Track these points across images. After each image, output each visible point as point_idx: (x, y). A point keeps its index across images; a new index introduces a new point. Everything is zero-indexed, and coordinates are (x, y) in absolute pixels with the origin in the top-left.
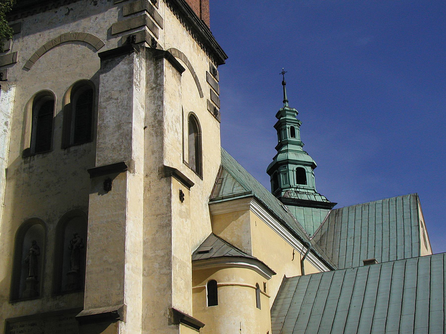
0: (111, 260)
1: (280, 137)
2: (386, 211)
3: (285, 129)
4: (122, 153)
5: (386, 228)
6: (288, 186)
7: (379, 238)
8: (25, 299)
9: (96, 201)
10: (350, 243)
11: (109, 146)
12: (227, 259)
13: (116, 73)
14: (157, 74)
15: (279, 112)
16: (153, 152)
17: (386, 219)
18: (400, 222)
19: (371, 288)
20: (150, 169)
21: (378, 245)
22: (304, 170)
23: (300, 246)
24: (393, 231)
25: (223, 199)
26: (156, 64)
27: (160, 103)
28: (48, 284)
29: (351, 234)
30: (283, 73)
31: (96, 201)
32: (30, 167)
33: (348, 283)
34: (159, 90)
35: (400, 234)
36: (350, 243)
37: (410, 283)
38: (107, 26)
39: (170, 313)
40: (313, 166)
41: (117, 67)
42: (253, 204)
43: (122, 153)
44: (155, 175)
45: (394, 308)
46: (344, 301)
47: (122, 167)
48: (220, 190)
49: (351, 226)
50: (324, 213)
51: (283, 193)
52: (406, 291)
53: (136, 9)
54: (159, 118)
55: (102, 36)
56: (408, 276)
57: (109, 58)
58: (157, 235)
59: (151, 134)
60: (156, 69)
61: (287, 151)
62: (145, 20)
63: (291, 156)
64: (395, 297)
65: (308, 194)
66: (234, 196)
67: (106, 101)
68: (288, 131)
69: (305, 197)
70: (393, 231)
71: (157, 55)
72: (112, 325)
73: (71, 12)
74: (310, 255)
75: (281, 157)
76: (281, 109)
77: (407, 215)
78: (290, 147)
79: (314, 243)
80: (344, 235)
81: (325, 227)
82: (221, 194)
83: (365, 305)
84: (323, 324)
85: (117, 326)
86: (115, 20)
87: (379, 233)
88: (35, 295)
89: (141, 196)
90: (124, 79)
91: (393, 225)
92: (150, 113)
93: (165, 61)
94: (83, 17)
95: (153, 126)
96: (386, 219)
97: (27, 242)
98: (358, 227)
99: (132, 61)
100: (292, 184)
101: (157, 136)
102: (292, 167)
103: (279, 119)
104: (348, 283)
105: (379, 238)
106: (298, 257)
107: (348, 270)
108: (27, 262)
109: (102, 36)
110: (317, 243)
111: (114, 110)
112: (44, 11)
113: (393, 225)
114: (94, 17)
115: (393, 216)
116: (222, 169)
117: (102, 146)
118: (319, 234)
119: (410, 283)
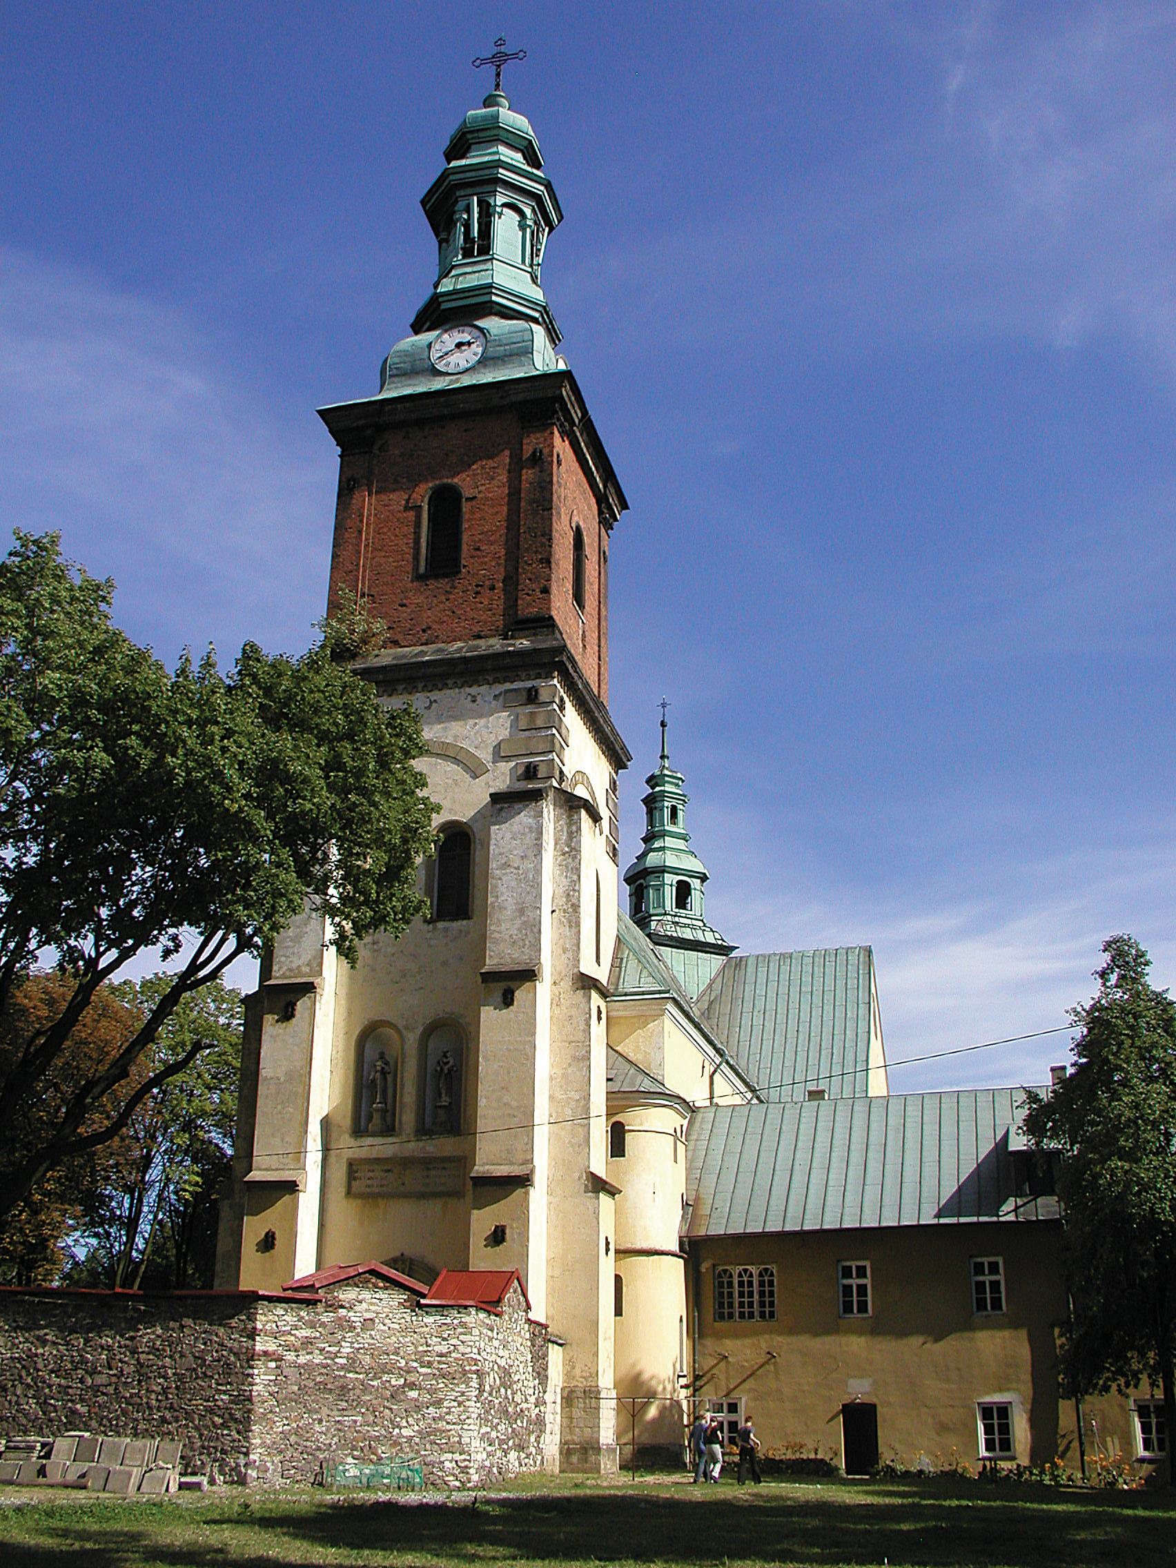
0: (514, 1104)
1: (651, 822)
2: (818, 971)
3: (662, 810)
4: (526, 950)
5: (817, 1000)
6: (661, 911)
7: (805, 1017)
8: (373, 1135)
9: (490, 1017)
10: (758, 1020)
11: (507, 937)
12: (642, 1095)
13: (515, 828)
14: (572, 833)
15: (653, 777)
16: (565, 950)
17: (818, 986)
18: (840, 993)
19: (823, 1138)
20: (560, 973)
21: (815, 1040)
22: (688, 884)
23: (711, 1052)
24: (828, 1008)
25: (626, 995)
26: (570, 816)
27: (575, 877)
28: (408, 1118)
29: (760, 1004)
30: (664, 705)
31: (490, 1017)
32: (374, 943)
33: (789, 1127)
34: (574, 858)
35: (840, 1013)
36: (758, 1020)
37: (876, 1136)
38: (492, 741)
39: (587, 1179)
40: (703, 878)
41: (517, 818)
42: (670, 1006)
43: (526, 950)
44: (566, 984)
45: (855, 1173)
46: (784, 1154)
47: (529, 975)
48: (619, 978)
49: (760, 991)
50: (717, 961)
51: (653, 924)
52: (871, 1147)
53: (539, 723)
54: (574, 901)
55: (485, 755)
56: (873, 1125)
57: (504, 802)
58: (569, 1071)
59: (561, 922)
60: (570, 825)
61: (663, 849)
62: (553, 744)
63: (671, 860)
64: (856, 1157)
65: (693, 927)
66: (643, 993)
67: (501, 869)
68: (667, 813)
69: (687, 934)
70: (828, 1008)
71: (573, 804)
72: (520, 1191)
73: (434, 705)
74: (724, 1067)
75: (653, 859)
76: (657, 773)
77: (852, 983)
78: (669, 842)
79: (698, 1013)
80: (748, 1006)
81: (717, 986)
82: (621, 986)
83: (814, 1165)
84: (756, 1187)
85: (527, 1193)
86: (504, 733)
87: (805, 1007)
88: (389, 1129)
89: (548, 1014)
90: (529, 839)
91: (829, 997)
92: (561, 891)
93: (583, 812)
94: (455, 718)
95: (565, 911)
96: (818, 986)
97: (369, 1053)
98: (772, 994)
99: (540, 814)
100: (668, 908)
101: (570, 927)
102: (670, 879)
103: (653, 788)
104: (789, 1127)
105: (805, 1017)
106: (709, 1069)
107: (788, 1105)
108: (374, 1081)
109: (485, 755)
110: (703, 1014)
111: (514, 883)
112: (390, 696)
113: (829, 997)
114: (471, 722)
115: (829, 981)
116: (619, 940)
117: (496, 935)
118: (706, 998)
119: (876, 1136)
